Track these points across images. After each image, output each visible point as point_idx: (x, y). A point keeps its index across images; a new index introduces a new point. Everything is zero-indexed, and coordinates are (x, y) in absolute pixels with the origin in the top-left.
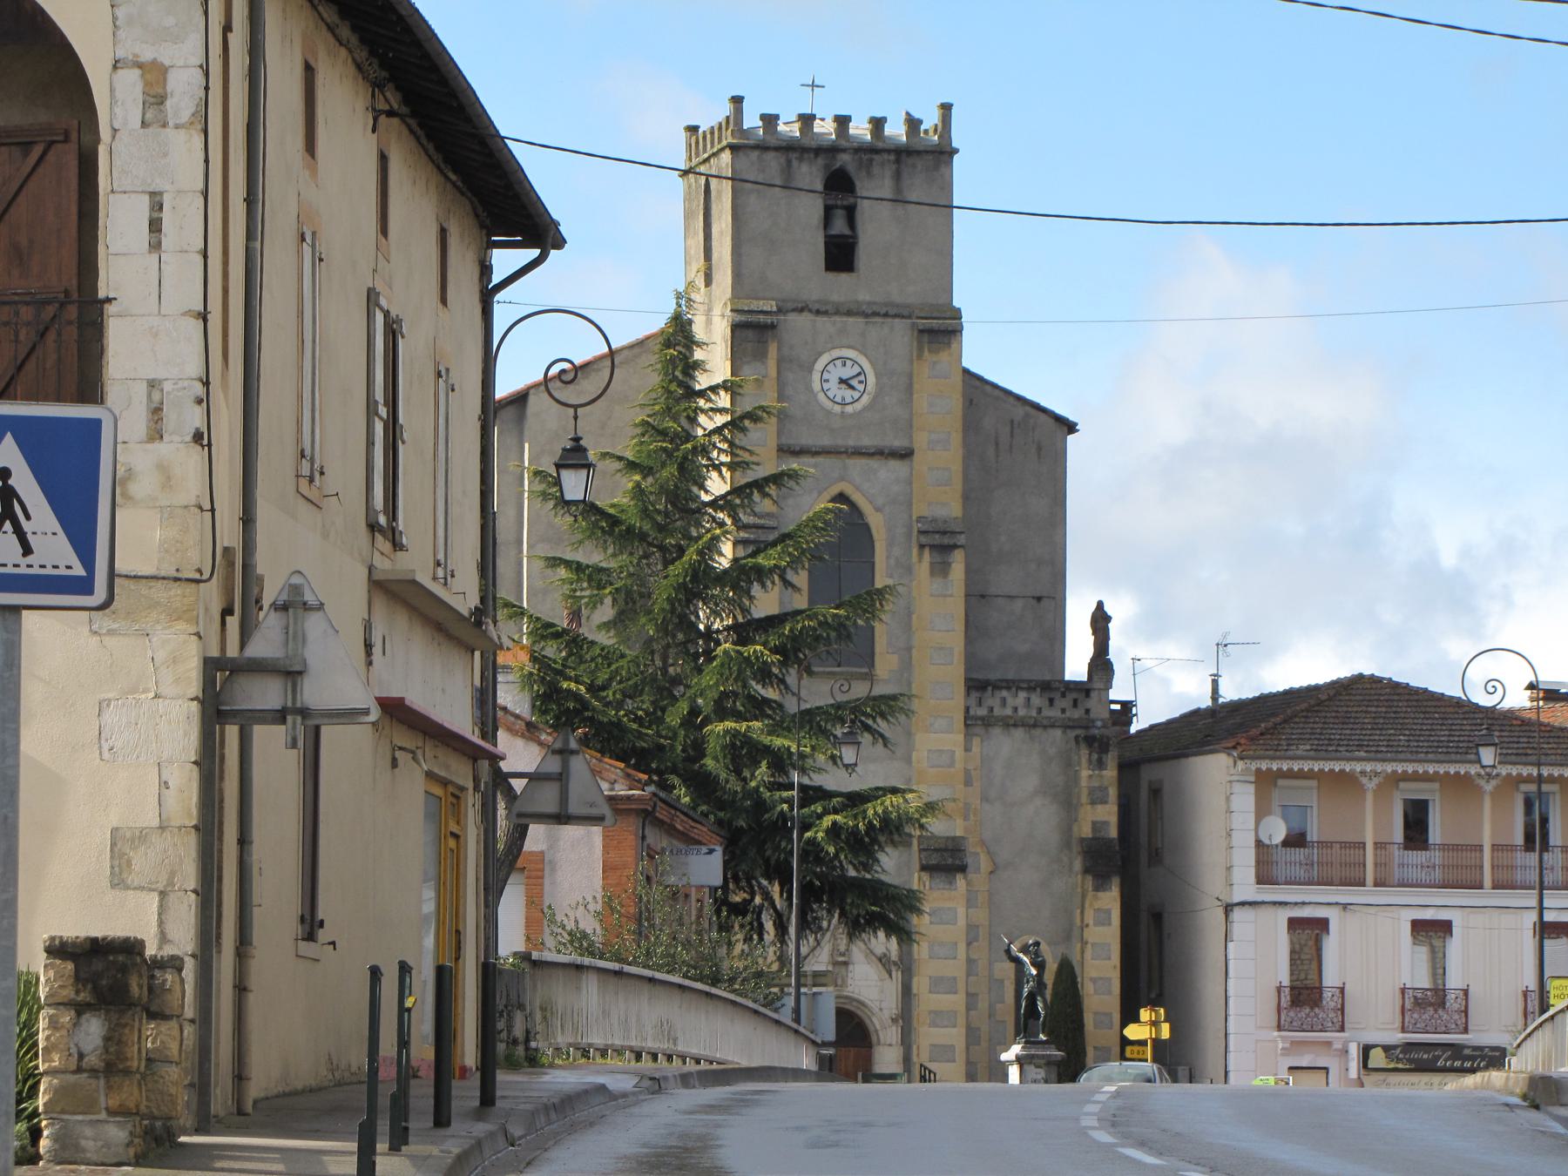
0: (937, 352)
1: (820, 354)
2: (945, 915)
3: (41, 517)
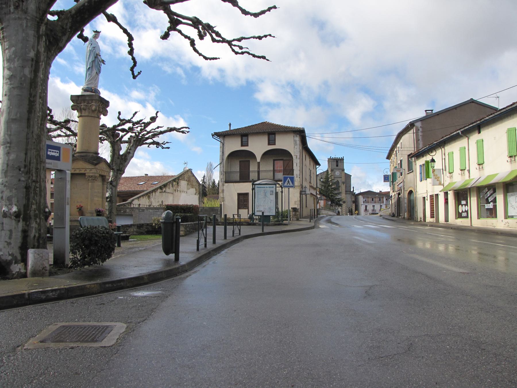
2: (344, 205)
3: (291, 183)
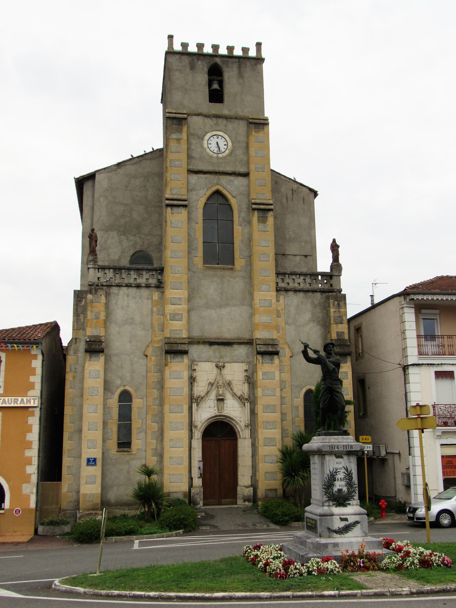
0: (258, 132)
1: (207, 133)
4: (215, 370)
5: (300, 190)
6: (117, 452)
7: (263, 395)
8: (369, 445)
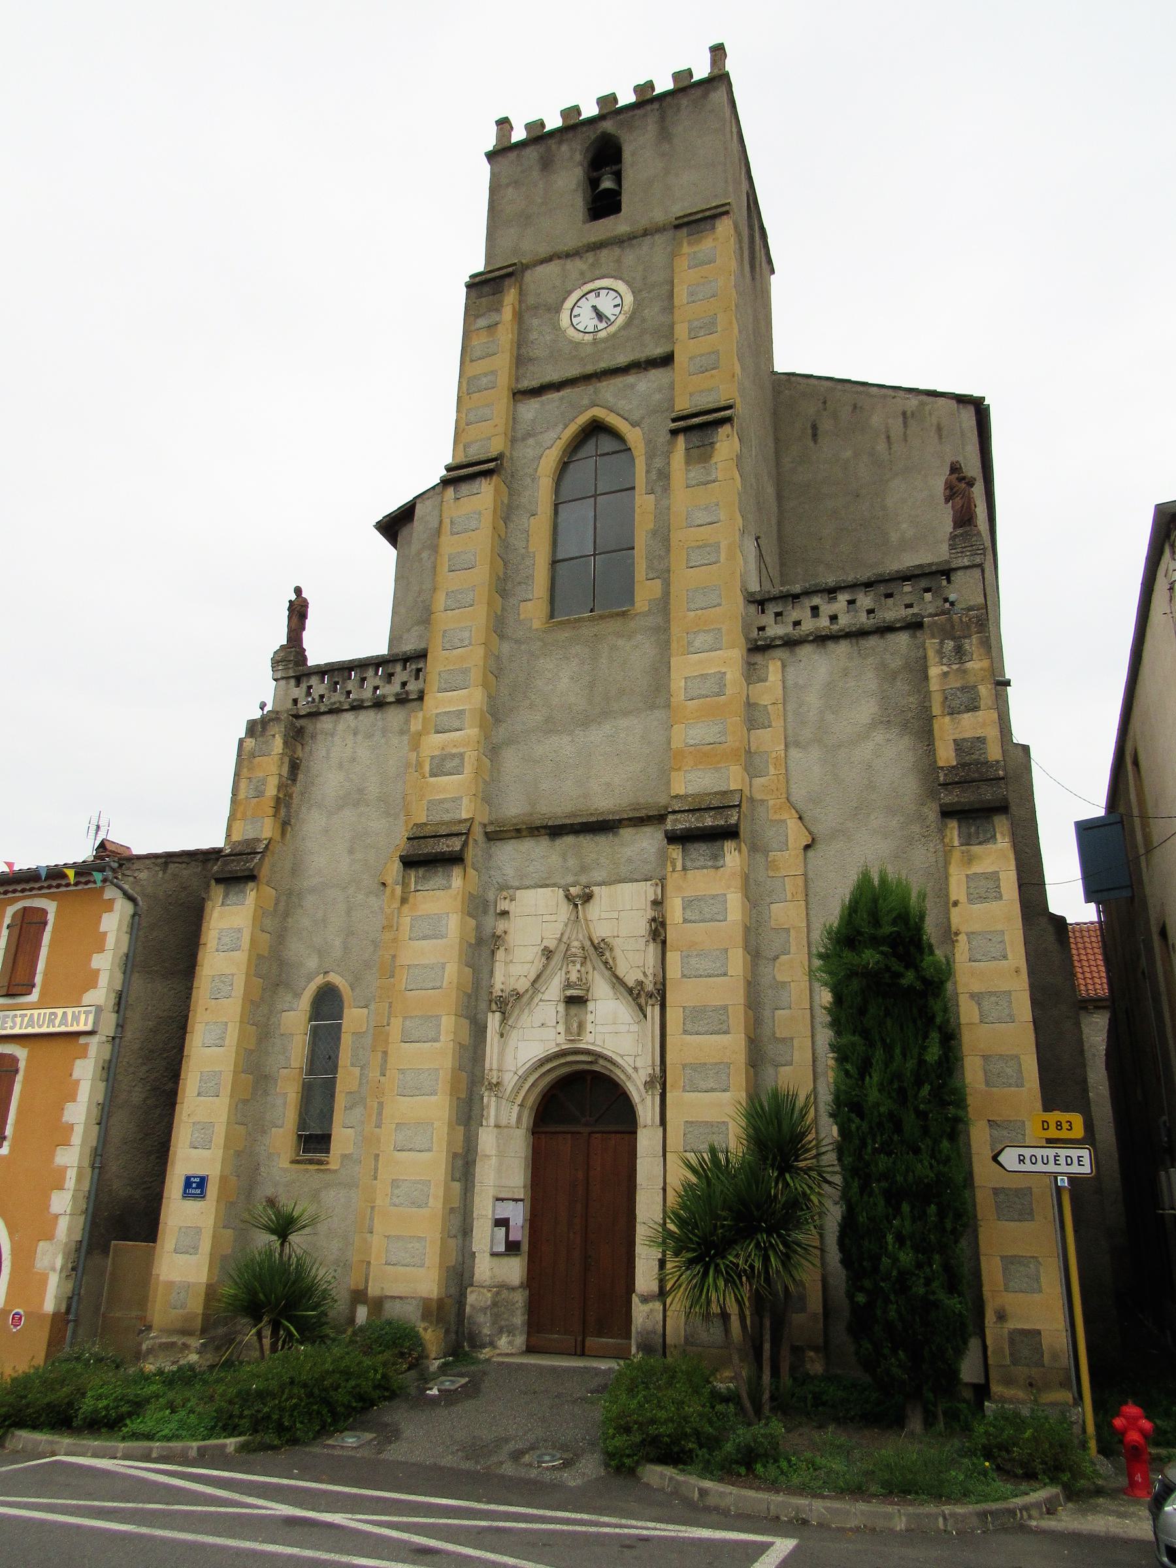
1: (570, 293)
4: (565, 910)
5: (927, 408)
6: (293, 1162)
7: (684, 976)
8: (1074, 1153)
